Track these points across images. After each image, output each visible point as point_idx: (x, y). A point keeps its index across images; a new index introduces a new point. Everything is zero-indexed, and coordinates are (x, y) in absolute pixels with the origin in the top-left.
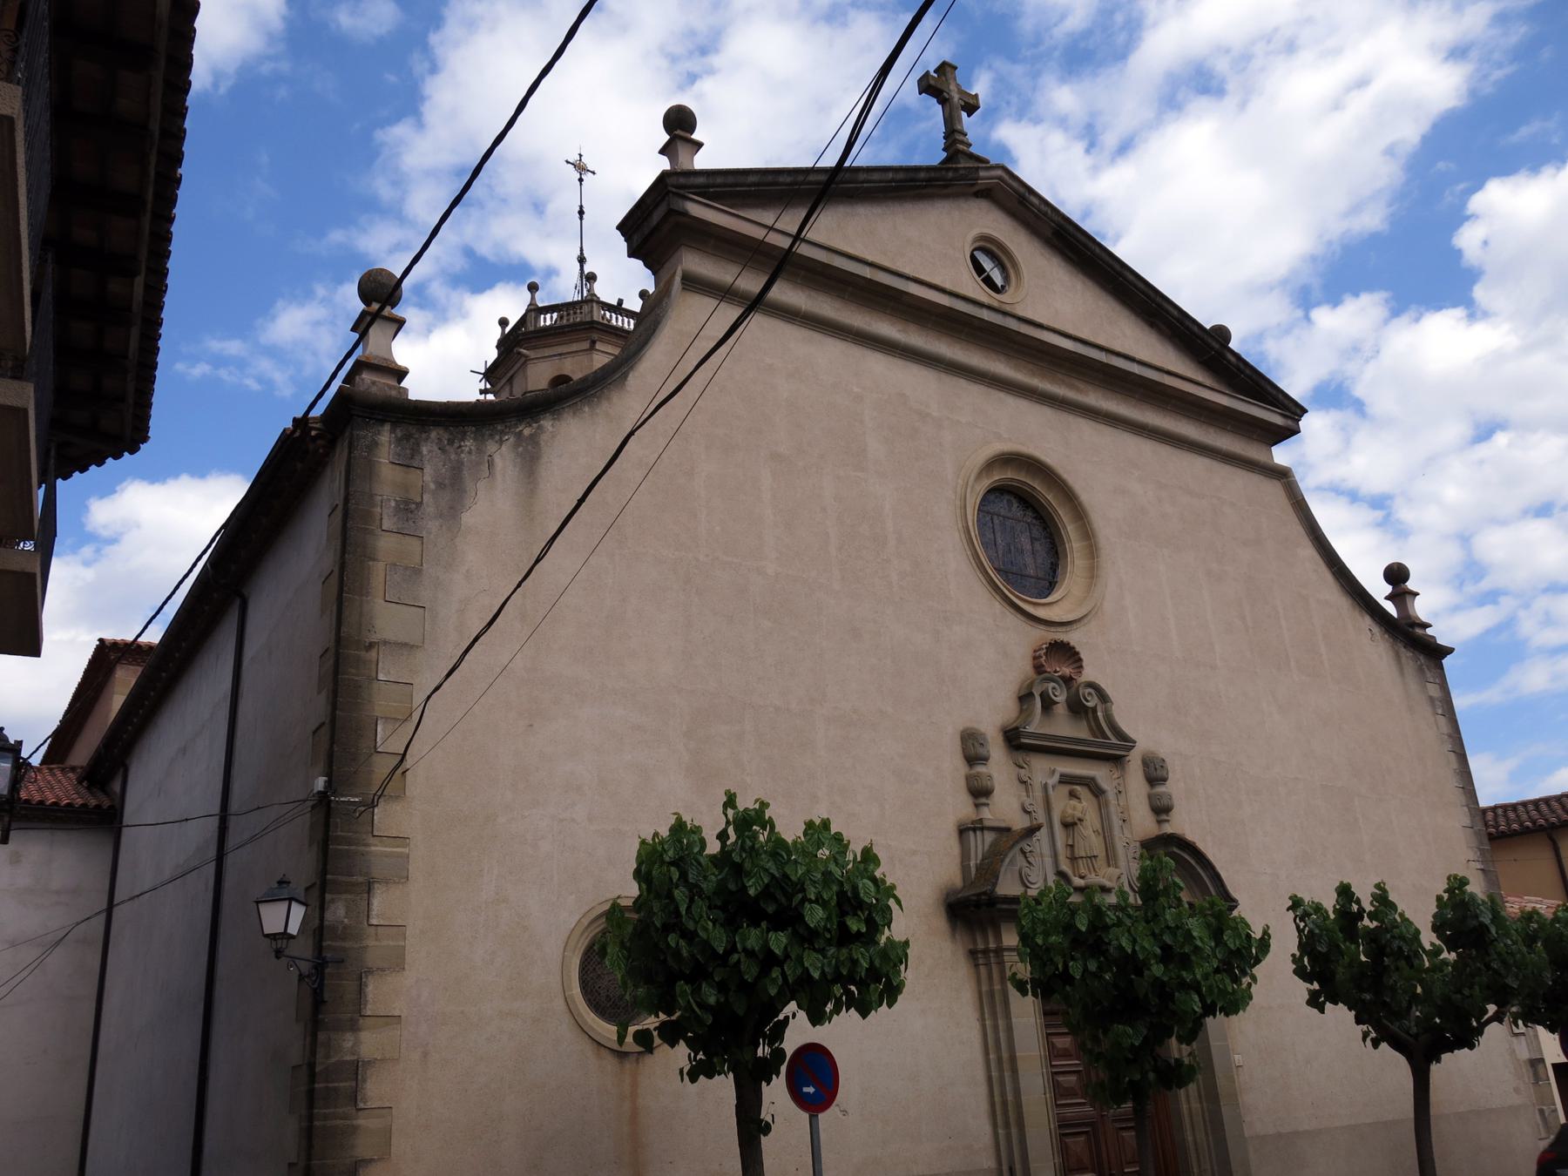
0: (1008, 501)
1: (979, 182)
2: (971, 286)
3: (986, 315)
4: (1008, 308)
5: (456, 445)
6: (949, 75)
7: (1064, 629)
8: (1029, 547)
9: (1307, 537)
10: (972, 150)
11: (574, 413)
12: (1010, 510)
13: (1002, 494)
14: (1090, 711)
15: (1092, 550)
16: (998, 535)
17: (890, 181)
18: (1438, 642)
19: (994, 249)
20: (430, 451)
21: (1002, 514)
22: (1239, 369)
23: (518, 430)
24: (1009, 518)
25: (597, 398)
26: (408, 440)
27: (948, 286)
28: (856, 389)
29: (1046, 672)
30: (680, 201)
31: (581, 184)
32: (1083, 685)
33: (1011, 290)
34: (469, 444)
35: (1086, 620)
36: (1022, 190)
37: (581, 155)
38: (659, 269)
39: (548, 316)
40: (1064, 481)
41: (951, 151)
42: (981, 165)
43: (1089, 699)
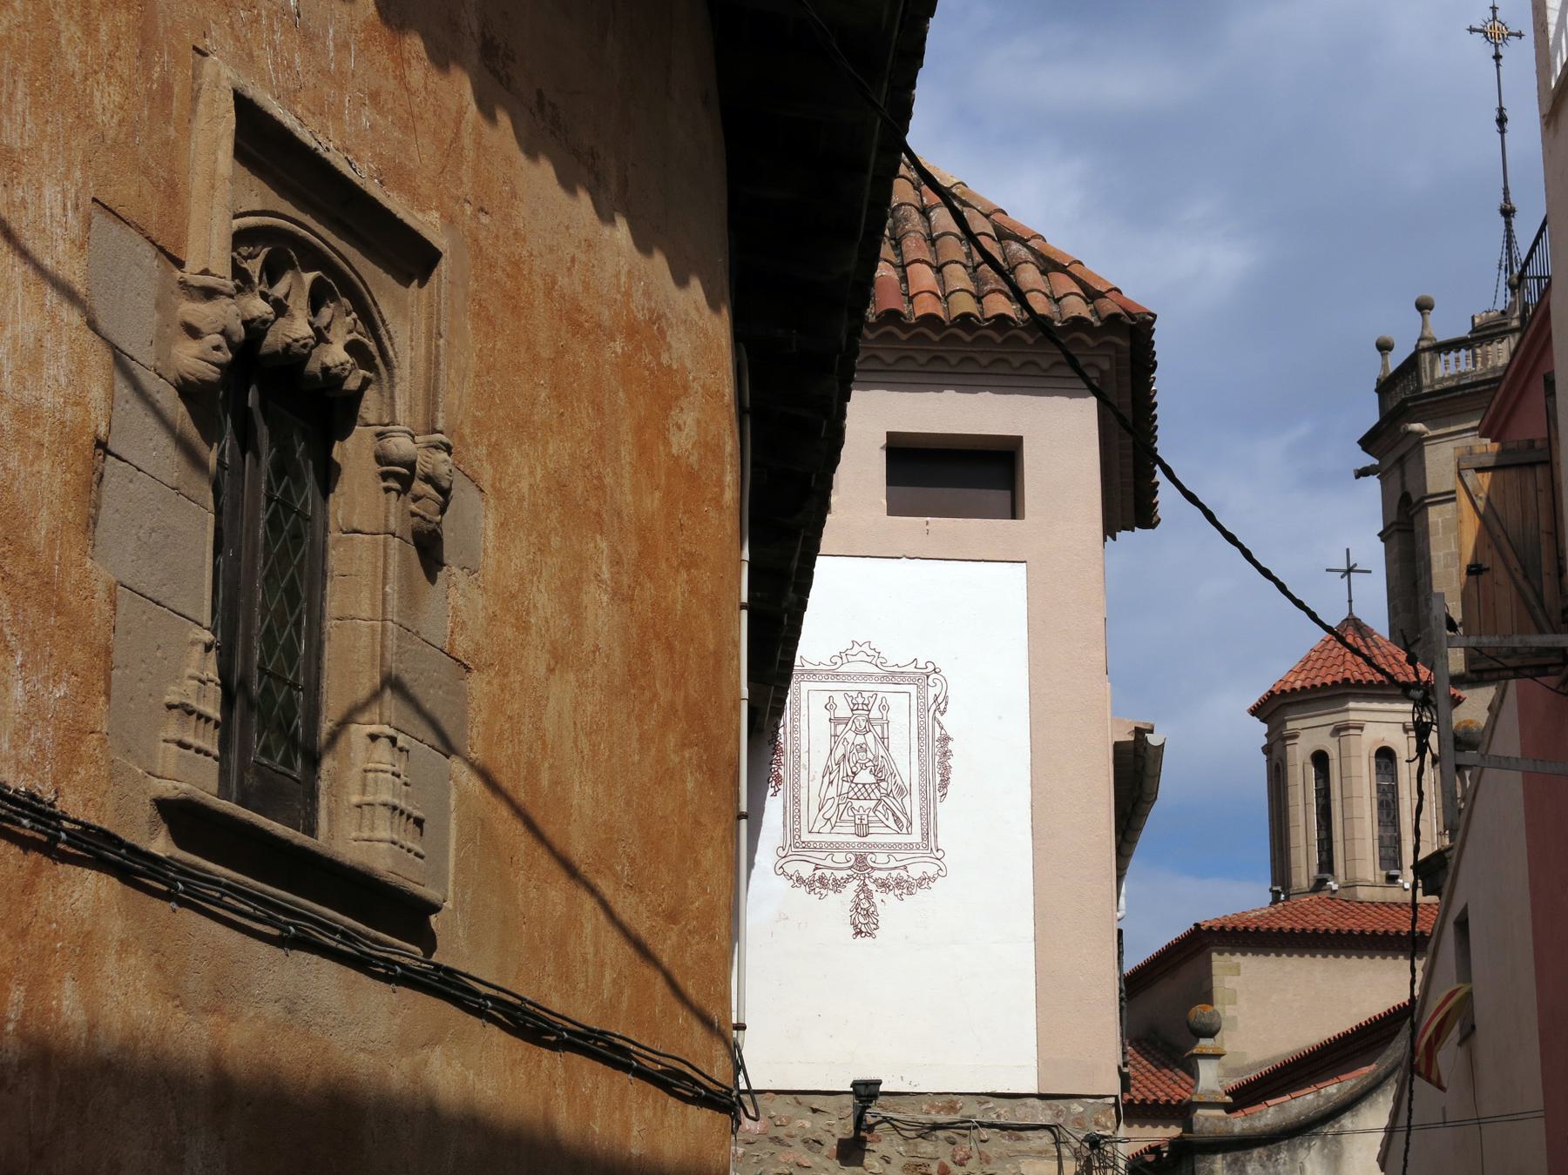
5: (1273, 1159)
11: (1371, 1106)
20: (1253, 1170)
26: (1236, 1164)
31: (1498, 65)
34: (1284, 1155)
37: (1494, 9)
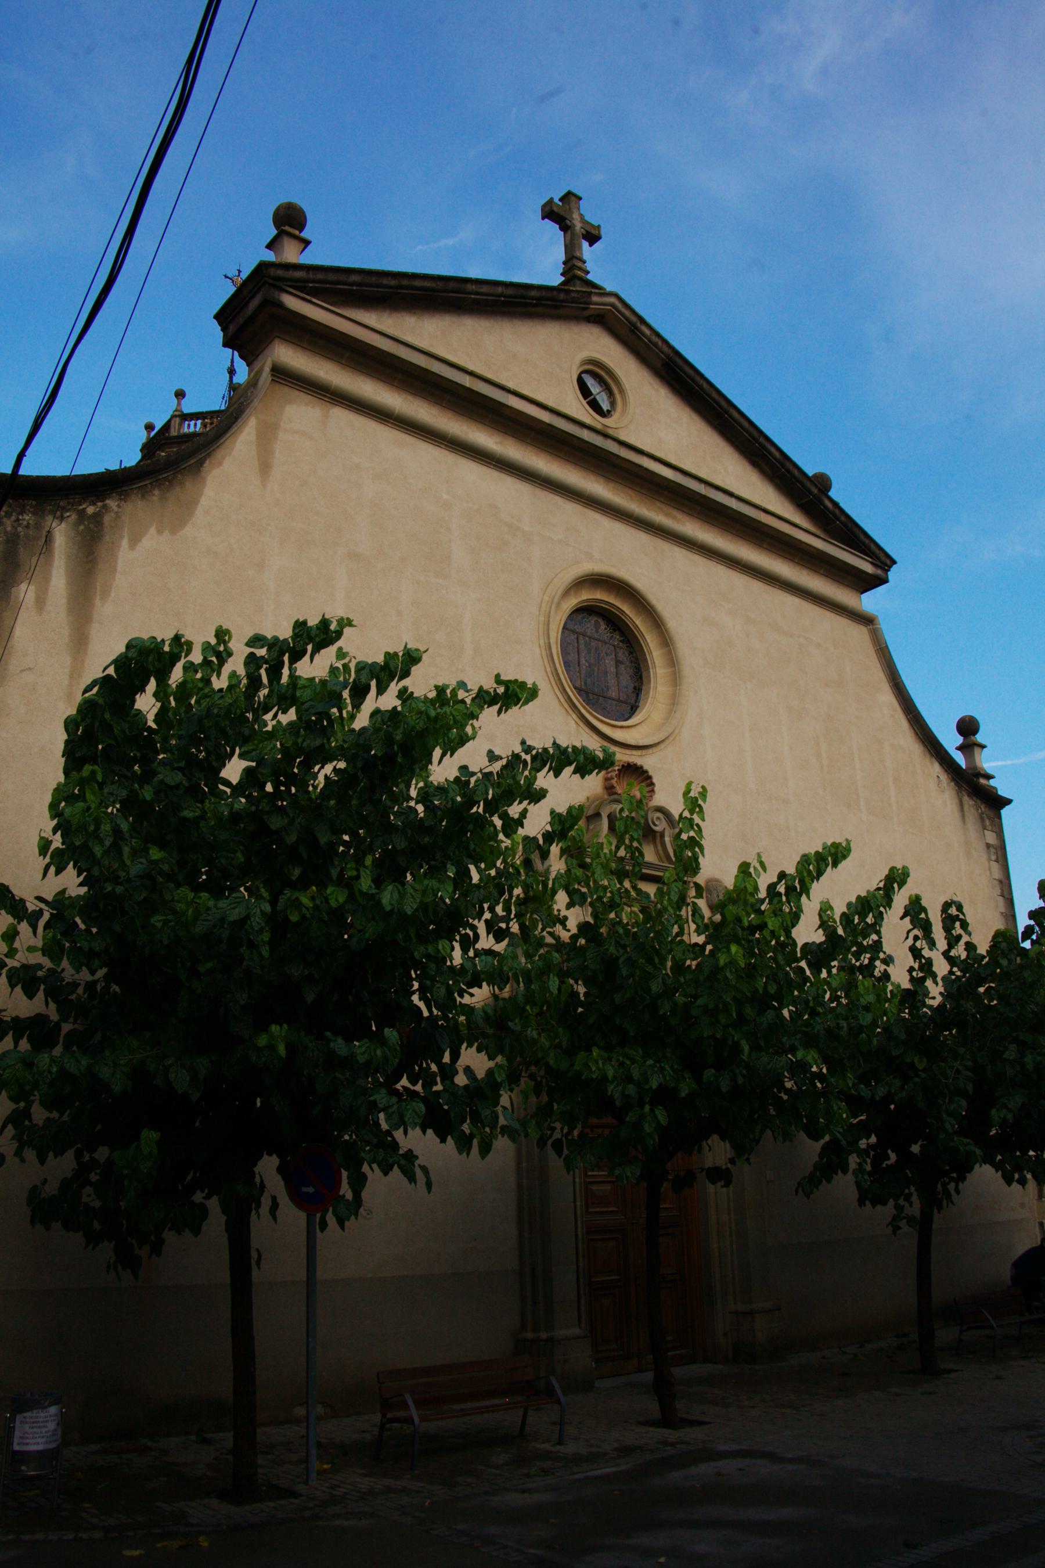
0: (596, 622)
1: (592, 306)
2: (576, 407)
3: (586, 435)
4: (610, 432)
5: (13, 518)
6: (573, 205)
7: (639, 753)
8: (613, 670)
9: (887, 683)
10: (590, 277)
12: (597, 632)
13: (590, 615)
14: (658, 835)
15: (676, 678)
16: (583, 654)
17: (500, 296)
18: (1000, 793)
19: (603, 373)
21: (588, 634)
22: (834, 515)
23: (81, 507)
24: (595, 639)
25: (169, 482)
27: (550, 403)
28: (445, 496)
29: (616, 793)
30: (277, 293)
32: (653, 809)
33: (616, 415)
35: (662, 746)
36: (634, 319)
38: (254, 360)
39: (192, 423)
40: (652, 607)
41: (568, 276)
42: (593, 290)
43: (657, 823)
